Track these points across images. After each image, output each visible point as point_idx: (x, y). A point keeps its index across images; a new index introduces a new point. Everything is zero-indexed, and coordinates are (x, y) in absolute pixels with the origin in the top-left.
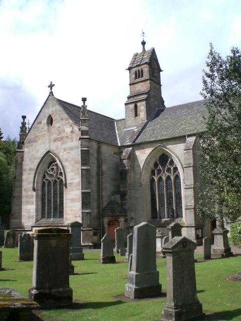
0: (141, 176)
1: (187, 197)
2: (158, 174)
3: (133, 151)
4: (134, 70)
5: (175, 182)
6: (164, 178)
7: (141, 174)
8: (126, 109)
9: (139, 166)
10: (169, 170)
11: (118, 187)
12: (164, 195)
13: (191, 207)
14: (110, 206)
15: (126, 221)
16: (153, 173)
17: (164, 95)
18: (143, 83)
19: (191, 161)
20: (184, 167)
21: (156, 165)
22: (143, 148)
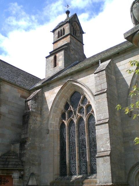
0: (48, 120)
1: (102, 133)
2: (69, 116)
3: (43, 93)
4: (57, 31)
5: (88, 124)
6: (75, 121)
7: (48, 118)
8: (47, 61)
9: (48, 108)
10: (81, 110)
11: (20, 134)
12: (75, 143)
13: (105, 153)
14: (6, 157)
15: (21, 177)
16: (63, 116)
17: (85, 53)
18: (65, 39)
19: (105, 86)
20: (95, 94)
21: (67, 106)
22: (53, 88)
